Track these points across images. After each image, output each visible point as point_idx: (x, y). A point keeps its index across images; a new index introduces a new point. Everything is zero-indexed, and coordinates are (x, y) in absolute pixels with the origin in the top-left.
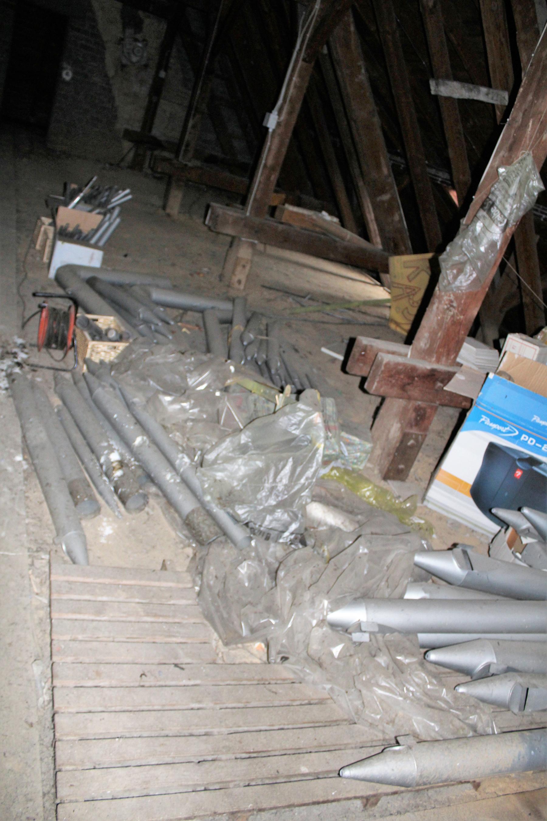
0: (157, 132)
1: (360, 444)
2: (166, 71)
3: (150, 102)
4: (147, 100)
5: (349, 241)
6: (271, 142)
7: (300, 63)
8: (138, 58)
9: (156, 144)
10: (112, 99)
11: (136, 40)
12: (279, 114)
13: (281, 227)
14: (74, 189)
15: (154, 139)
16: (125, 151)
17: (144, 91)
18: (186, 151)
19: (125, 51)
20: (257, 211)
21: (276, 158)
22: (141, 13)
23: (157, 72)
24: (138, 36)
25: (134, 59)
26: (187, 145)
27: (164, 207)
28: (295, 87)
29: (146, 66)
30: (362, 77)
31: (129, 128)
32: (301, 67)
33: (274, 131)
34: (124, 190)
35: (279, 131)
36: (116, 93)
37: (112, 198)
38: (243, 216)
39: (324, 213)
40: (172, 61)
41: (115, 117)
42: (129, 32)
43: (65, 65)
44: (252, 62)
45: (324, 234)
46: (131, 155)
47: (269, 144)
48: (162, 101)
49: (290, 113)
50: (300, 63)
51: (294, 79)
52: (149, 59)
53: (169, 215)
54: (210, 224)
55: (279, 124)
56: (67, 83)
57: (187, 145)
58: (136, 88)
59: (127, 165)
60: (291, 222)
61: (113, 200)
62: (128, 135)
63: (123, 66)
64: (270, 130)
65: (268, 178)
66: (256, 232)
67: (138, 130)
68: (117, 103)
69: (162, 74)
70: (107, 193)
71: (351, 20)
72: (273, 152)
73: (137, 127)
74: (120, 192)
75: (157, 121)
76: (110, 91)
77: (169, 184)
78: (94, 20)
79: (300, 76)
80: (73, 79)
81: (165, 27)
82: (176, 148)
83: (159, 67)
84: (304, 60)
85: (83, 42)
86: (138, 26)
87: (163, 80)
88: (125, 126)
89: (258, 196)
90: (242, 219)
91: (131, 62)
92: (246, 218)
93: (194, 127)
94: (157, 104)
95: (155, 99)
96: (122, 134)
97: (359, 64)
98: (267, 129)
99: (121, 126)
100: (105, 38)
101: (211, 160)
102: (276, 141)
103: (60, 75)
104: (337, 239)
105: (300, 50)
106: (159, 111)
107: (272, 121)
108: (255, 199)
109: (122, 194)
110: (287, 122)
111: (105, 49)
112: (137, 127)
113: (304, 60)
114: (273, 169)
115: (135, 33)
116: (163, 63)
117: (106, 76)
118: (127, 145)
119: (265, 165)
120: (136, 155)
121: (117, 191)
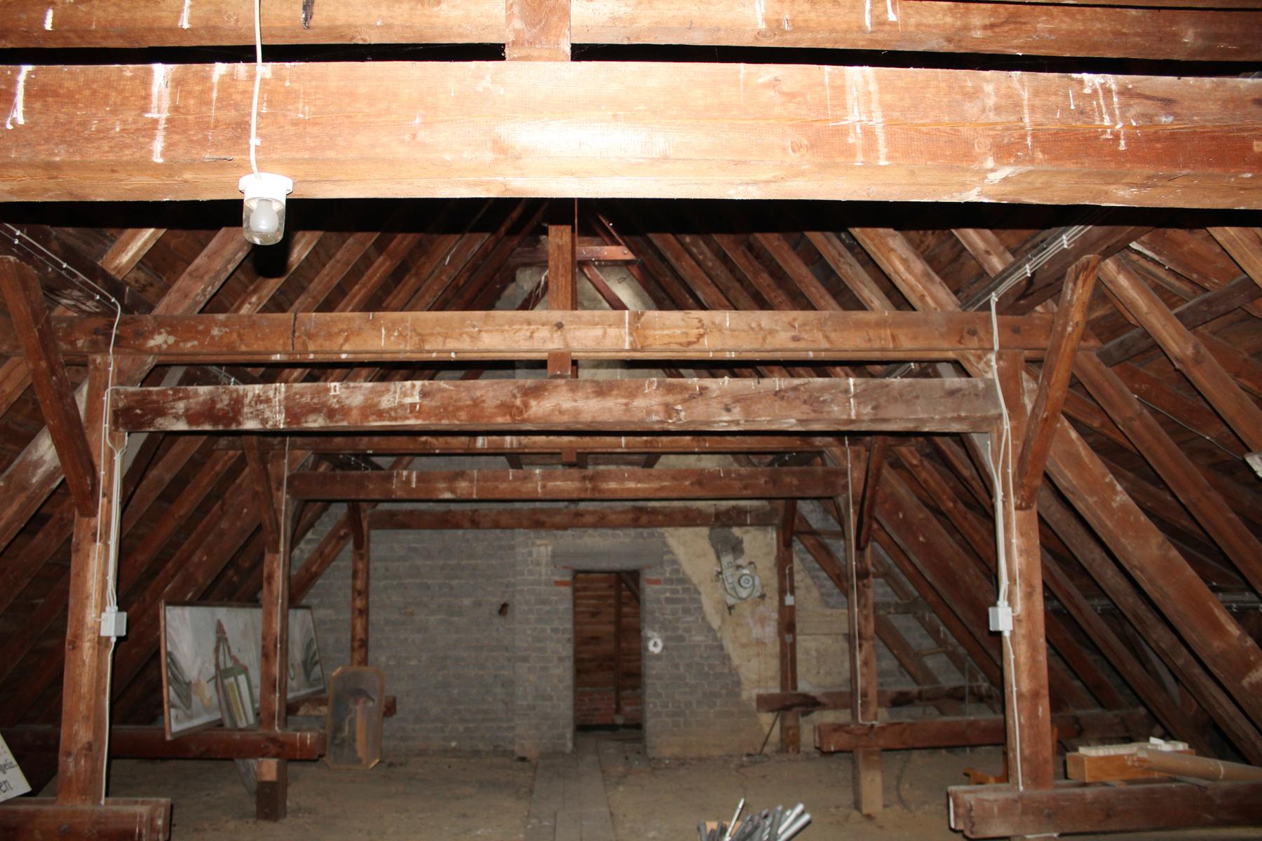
0: (805, 686)
1: (642, 515)
2: (792, 593)
3: (783, 644)
4: (778, 643)
5: (1226, 778)
6: (1015, 653)
7: (1014, 515)
8: (748, 591)
9: (810, 704)
10: (726, 659)
11: (739, 567)
12: (1011, 602)
13: (1089, 792)
14: (712, 831)
15: (805, 696)
16: (767, 729)
17: (770, 632)
18: (864, 704)
19: (728, 586)
20: (1035, 777)
21: (1033, 676)
22: (736, 531)
23: (782, 601)
24: (740, 562)
25: (744, 593)
26: (864, 695)
27: (857, 805)
28: (1021, 553)
29: (763, 597)
30: (1121, 497)
31: (762, 691)
32: (1018, 521)
33: (1013, 633)
34: (793, 807)
35: (1022, 631)
36: (730, 647)
37: (779, 826)
38: (1010, 795)
39: (1153, 740)
40: (797, 577)
41: (738, 683)
42: (727, 559)
43: (649, 633)
44: (921, 539)
45: (1174, 780)
46: (776, 731)
47: (1012, 657)
48: (798, 638)
49: (1029, 596)
50: (1014, 515)
51: (1014, 541)
52: (763, 586)
53: (869, 817)
54: (961, 827)
55: (1017, 620)
56: (658, 657)
57: (864, 695)
58: (757, 632)
59: (774, 748)
60: (1105, 779)
61: (780, 831)
62: (764, 702)
63: (730, 608)
64: (1007, 634)
65: (1033, 714)
66: (1049, 816)
67: (777, 691)
68: (736, 662)
69: (789, 600)
70: (768, 822)
71: (1066, 423)
72: (1024, 668)
73: (774, 688)
74: (788, 813)
75: (801, 669)
76: (721, 648)
77: (854, 762)
78: (674, 562)
79: (1022, 534)
80: (664, 648)
81: (775, 536)
82: (845, 699)
83: (782, 592)
84: (1018, 508)
85: (668, 595)
86: (736, 548)
87: (792, 608)
88: (755, 692)
89: (1027, 752)
90: (1015, 801)
91: (741, 599)
92: (1021, 797)
93: (866, 663)
94: (793, 645)
95: (788, 638)
96: (754, 704)
97: (1107, 480)
98: (999, 634)
99: (750, 693)
100: (695, 580)
101: (901, 700)
102: (1023, 648)
103: (647, 649)
104: (1204, 783)
105: (1006, 495)
106: (800, 656)
107: (1003, 618)
108: (1023, 759)
109: (791, 815)
110: (1030, 614)
111: (699, 593)
112: (774, 688)
113: (1018, 508)
114: (1035, 695)
115: (735, 559)
116: (786, 585)
117: (710, 629)
118: (767, 718)
119: (1020, 696)
120: (783, 729)
121: (783, 812)
